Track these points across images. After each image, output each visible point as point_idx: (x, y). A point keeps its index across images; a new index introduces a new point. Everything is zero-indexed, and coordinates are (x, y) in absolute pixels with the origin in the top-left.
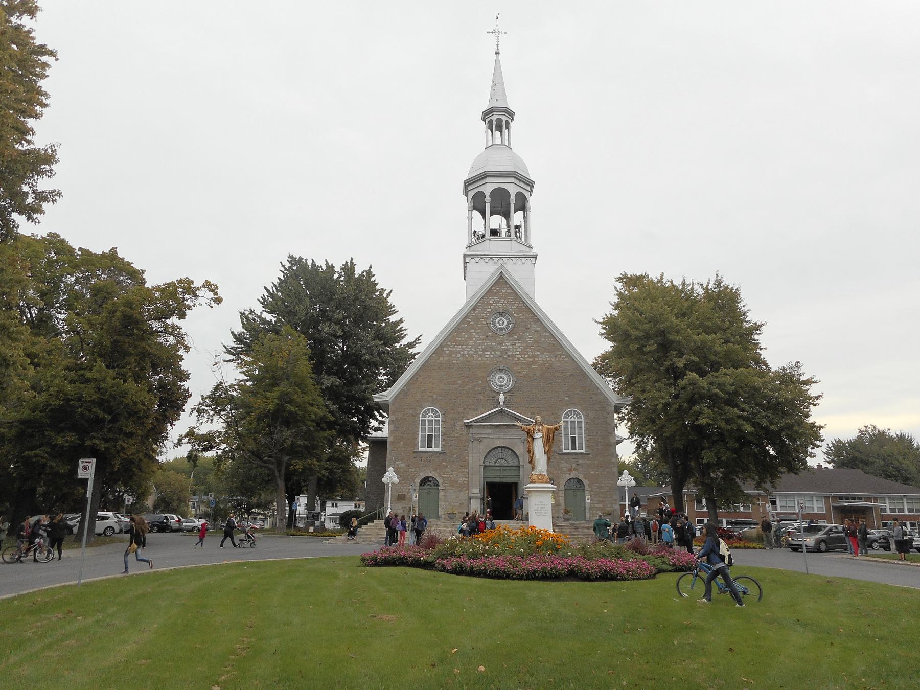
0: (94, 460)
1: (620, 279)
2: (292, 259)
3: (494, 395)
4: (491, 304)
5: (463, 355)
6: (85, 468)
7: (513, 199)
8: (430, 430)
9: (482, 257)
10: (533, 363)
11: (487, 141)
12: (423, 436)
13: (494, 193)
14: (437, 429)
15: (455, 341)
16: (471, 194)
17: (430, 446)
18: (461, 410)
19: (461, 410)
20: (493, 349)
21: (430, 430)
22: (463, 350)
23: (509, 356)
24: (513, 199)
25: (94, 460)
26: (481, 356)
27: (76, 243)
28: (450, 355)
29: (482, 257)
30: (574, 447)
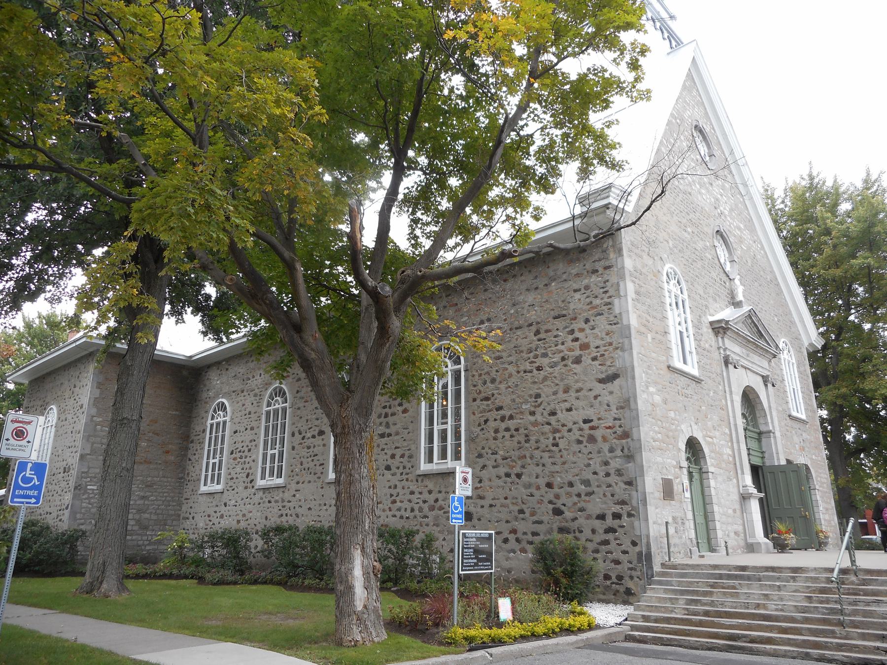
3: (725, 278)
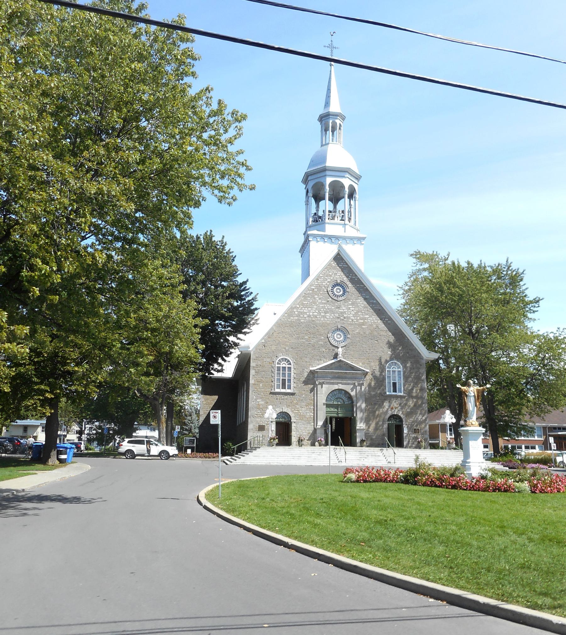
0: (219, 411)
1: (468, 263)
2: (419, 256)
4: (331, 276)
5: (309, 316)
6: (215, 417)
7: (347, 190)
8: (284, 374)
9: (323, 237)
10: (363, 324)
11: (322, 142)
12: (278, 380)
13: (333, 184)
14: (290, 375)
15: (303, 304)
16: (311, 184)
17: (284, 387)
18: (307, 360)
19: (307, 360)
20: (332, 312)
21: (284, 374)
22: (309, 311)
23: (345, 318)
24: (347, 190)
25: (219, 411)
26: (324, 317)
27: (422, 251)
28: (298, 316)
29: (323, 237)
30: (395, 391)
